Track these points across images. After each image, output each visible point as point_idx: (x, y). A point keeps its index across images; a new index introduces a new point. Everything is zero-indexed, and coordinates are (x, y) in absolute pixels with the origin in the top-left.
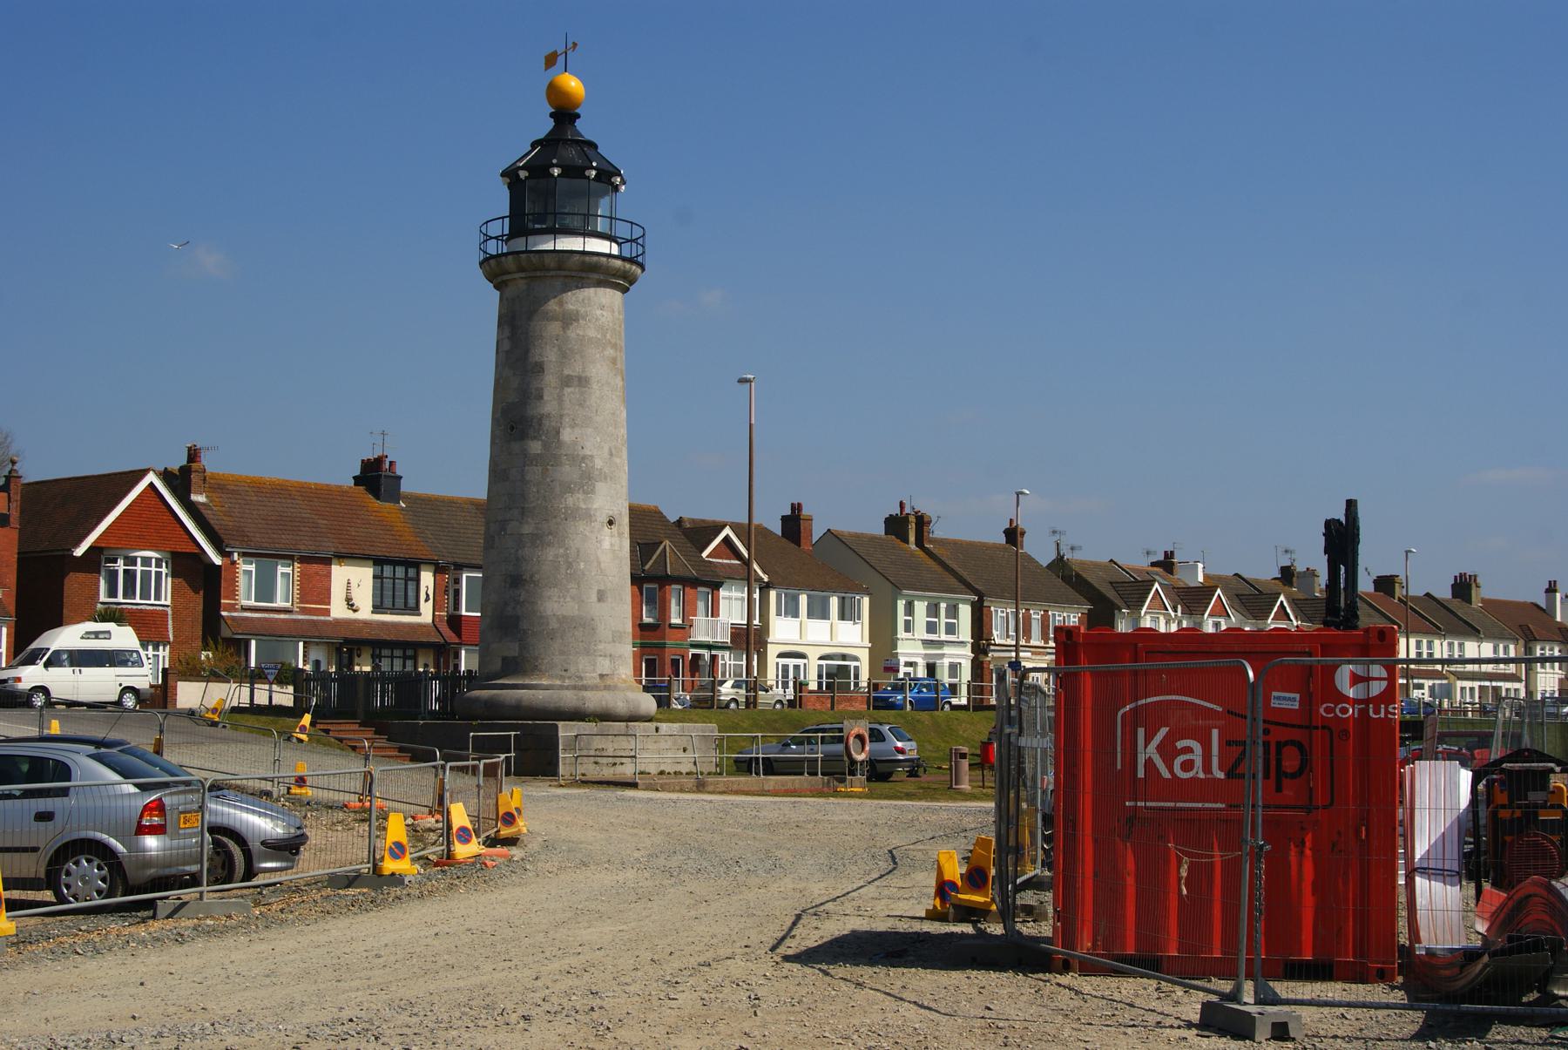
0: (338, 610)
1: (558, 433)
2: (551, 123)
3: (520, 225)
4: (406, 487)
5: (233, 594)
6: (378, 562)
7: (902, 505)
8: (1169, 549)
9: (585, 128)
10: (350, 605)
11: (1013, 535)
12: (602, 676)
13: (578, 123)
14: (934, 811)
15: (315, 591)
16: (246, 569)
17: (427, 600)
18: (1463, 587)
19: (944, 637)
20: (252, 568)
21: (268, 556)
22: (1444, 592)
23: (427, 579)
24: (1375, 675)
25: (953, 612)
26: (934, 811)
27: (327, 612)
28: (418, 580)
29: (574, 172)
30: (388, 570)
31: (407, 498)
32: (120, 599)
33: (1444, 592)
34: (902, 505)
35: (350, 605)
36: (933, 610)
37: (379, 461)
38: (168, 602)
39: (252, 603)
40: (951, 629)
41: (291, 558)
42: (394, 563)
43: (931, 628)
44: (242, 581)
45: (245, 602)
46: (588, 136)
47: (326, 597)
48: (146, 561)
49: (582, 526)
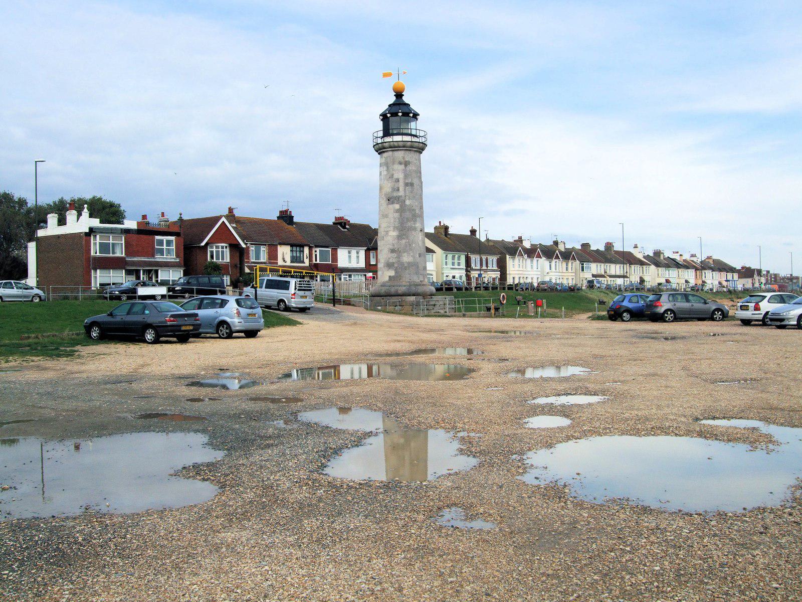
0: (280, 262)
1: (405, 202)
2: (395, 98)
3: (387, 132)
4: (295, 220)
5: (248, 258)
6: (292, 246)
7: (440, 222)
8: (520, 235)
9: (406, 99)
10: (284, 261)
11: (473, 232)
12: (421, 281)
13: (403, 98)
14: (416, 328)
15: (273, 256)
16: (252, 248)
17: (307, 258)
18: (609, 246)
19: (457, 267)
20: (253, 249)
21: (258, 245)
22: (602, 248)
23: (306, 250)
24: (358, 278)
25: (459, 258)
26: (416, 328)
27: (277, 263)
28: (303, 251)
29: (406, 114)
30: (294, 249)
31: (296, 223)
32: (215, 260)
33: (602, 248)
34: (440, 222)
35: (284, 261)
36: (453, 258)
37: (286, 211)
38: (228, 261)
39: (254, 261)
40: (459, 264)
41: (265, 245)
42: (296, 246)
43: (453, 264)
44: (251, 253)
45: (252, 260)
46: (407, 102)
47: (276, 258)
48: (222, 247)
49: (413, 233)
